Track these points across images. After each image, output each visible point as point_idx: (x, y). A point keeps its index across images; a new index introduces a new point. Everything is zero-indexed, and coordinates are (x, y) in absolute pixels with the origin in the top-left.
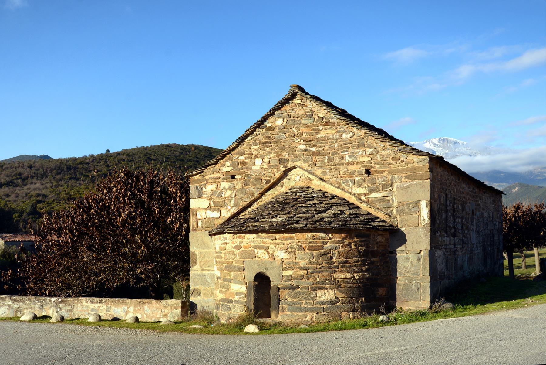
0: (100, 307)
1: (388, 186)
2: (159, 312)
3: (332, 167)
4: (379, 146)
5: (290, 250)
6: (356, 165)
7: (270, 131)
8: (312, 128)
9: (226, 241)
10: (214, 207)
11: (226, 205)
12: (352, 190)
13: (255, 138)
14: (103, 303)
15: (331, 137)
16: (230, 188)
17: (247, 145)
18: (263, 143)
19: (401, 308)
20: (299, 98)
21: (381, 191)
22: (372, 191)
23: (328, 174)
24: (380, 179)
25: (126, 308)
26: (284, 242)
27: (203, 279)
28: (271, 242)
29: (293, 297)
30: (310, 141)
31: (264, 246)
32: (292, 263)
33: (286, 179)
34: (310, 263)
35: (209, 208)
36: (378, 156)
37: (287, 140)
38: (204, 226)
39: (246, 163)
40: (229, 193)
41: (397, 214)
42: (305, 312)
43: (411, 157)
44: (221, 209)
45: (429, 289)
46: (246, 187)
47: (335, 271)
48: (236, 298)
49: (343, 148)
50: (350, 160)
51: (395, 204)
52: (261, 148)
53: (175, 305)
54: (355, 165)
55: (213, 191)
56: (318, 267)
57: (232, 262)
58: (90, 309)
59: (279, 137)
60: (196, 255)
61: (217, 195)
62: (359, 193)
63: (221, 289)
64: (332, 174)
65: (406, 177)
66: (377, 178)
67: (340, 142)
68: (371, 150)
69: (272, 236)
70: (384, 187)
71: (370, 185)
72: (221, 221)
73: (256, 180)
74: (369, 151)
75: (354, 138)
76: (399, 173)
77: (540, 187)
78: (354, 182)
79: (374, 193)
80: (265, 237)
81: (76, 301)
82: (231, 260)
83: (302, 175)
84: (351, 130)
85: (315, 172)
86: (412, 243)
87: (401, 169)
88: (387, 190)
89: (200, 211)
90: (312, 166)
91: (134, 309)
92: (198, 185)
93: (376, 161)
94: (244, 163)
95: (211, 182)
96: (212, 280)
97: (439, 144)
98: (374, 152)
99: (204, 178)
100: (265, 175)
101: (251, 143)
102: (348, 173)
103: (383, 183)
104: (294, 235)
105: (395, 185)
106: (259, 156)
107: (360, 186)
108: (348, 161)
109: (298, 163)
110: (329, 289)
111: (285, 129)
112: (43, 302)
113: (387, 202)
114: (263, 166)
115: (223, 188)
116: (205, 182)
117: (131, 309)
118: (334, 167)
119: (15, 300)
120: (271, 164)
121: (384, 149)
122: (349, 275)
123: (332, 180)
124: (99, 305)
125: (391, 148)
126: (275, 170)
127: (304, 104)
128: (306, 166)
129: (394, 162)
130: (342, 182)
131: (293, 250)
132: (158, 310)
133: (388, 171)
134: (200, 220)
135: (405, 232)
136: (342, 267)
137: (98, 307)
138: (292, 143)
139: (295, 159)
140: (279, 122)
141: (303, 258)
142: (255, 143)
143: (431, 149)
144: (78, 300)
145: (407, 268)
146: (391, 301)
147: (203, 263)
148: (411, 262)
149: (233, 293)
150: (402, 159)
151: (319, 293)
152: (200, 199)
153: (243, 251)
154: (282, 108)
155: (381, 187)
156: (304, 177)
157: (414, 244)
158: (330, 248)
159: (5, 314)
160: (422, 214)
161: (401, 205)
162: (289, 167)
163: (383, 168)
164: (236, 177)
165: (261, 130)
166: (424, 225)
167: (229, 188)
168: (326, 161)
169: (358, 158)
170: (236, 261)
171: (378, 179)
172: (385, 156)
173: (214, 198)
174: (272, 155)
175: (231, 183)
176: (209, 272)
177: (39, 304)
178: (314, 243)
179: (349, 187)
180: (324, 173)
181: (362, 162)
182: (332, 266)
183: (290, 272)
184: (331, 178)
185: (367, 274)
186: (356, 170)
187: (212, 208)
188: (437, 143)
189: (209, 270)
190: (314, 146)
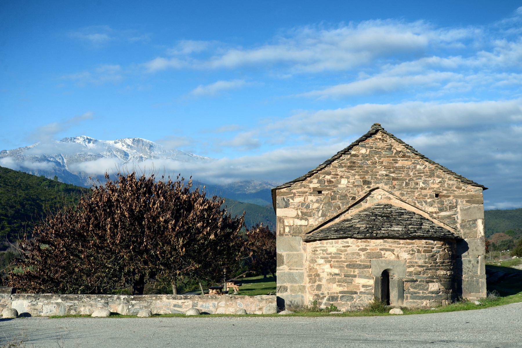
0: (184, 303)
1: (454, 208)
2: (254, 306)
3: (409, 190)
4: (445, 177)
5: (412, 253)
6: (429, 190)
7: (354, 158)
8: (391, 159)
9: (347, 245)
11: (314, 215)
13: (340, 162)
14: (189, 299)
15: (408, 167)
16: (317, 201)
17: (333, 167)
18: (349, 167)
19: (466, 298)
20: (380, 134)
21: (448, 211)
22: (441, 210)
23: (405, 195)
24: (447, 202)
25: (217, 303)
26: (407, 246)
28: (397, 246)
29: (415, 288)
30: (390, 168)
33: (370, 197)
34: (425, 263)
35: (297, 217)
37: (370, 166)
38: (292, 232)
39: (333, 182)
40: (316, 205)
41: (461, 229)
42: (422, 299)
43: (470, 187)
44: (309, 218)
45: (486, 284)
46: (333, 201)
47: (439, 269)
48: (363, 290)
49: (417, 176)
50: (424, 186)
51: (459, 221)
52: (346, 170)
53: (270, 300)
54: (427, 190)
55: (300, 203)
56: (429, 265)
57: (357, 261)
58: (173, 305)
59: (363, 163)
60: (283, 256)
61: (305, 206)
62: (431, 211)
64: (409, 195)
65: (467, 202)
66: (444, 200)
67: (415, 171)
68: (440, 179)
69: (398, 241)
70: (451, 208)
71: (439, 205)
74: (438, 180)
75: (426, 169)
77: (240, 203)
78: (426, 202)
79: (443, 211)
80: (391, 242)
81: (155, 298)
82: (354, 260)
83: (384, 195)
84: (424, 163)
85: (394, 193)
88: (453, 210)
90: (392, 188)
91: (226, 305)
92: (285, 197)
93: (444, 188)
94: (330, 182)
95: (299, 196)
96: (300, 278)
97: (132, 145)
98: (442, 181)
99: (291, 191)
100: (350, 193)
101: (337, 166)
102: (422, 195)
103: (450, 205)
104: (414, 241)
105: (459, 207)
106: (344, 177)
107: (432, 206)
109: (380, 185)
111: (368, 157)
112: (109, 299)
113: (453, 219)
114: (349, 186)
115: (311, 201)
116: (293, 195)
117: (223, 303)
118: (410, 190)
119: (67, 298)
120: (356, 184)
121: (450, 179)
122: (445, 272)
123: (409, 200)
124: (183, 301)
125: (455, 180)
126: (360, 189)
127: (384, 139)
128: (386, 187)
129: (458, 190)
131: (413, 252)
132: (252, 304)
133: (453, 196)
134: (287, 227)
135: (467, 242)
136: (442, 266)
137: (182, 303)
138: (374, 169)
139: (378, 181)
140: (363, 151)
141: (420, 259)
142: (341, 166)
143: (124, 151)
144: (156, 297)
145: (470, 268)
148: (472, 264)
149: (358, 286)
150: (463, 188)
151: (431, 285)
152: (286, 209)
153: (369, 252)
154: (366, 140)
155: (448, 208)
156: (385, 197)
157: (474, 251)
158: (436, 251)
159: (50, 313)
160: (479, 229)
161: (463, 221)
165: (346, 156)
166: (481, 237)
167: (316, 201)
168: (404, 185)
171: (446, 201)
173: (301, 209)
174: (357, 177)
175: (318, 197)
176: (297, 271)
177: (103, 301)
178: (427, 248)
180: (402, 194)
181: (433, 188)
182: (437, 265)
183: (412, 269)
184: (408, 199)
188: (130, 144)
189: (297, 270)
190: (394, 172)
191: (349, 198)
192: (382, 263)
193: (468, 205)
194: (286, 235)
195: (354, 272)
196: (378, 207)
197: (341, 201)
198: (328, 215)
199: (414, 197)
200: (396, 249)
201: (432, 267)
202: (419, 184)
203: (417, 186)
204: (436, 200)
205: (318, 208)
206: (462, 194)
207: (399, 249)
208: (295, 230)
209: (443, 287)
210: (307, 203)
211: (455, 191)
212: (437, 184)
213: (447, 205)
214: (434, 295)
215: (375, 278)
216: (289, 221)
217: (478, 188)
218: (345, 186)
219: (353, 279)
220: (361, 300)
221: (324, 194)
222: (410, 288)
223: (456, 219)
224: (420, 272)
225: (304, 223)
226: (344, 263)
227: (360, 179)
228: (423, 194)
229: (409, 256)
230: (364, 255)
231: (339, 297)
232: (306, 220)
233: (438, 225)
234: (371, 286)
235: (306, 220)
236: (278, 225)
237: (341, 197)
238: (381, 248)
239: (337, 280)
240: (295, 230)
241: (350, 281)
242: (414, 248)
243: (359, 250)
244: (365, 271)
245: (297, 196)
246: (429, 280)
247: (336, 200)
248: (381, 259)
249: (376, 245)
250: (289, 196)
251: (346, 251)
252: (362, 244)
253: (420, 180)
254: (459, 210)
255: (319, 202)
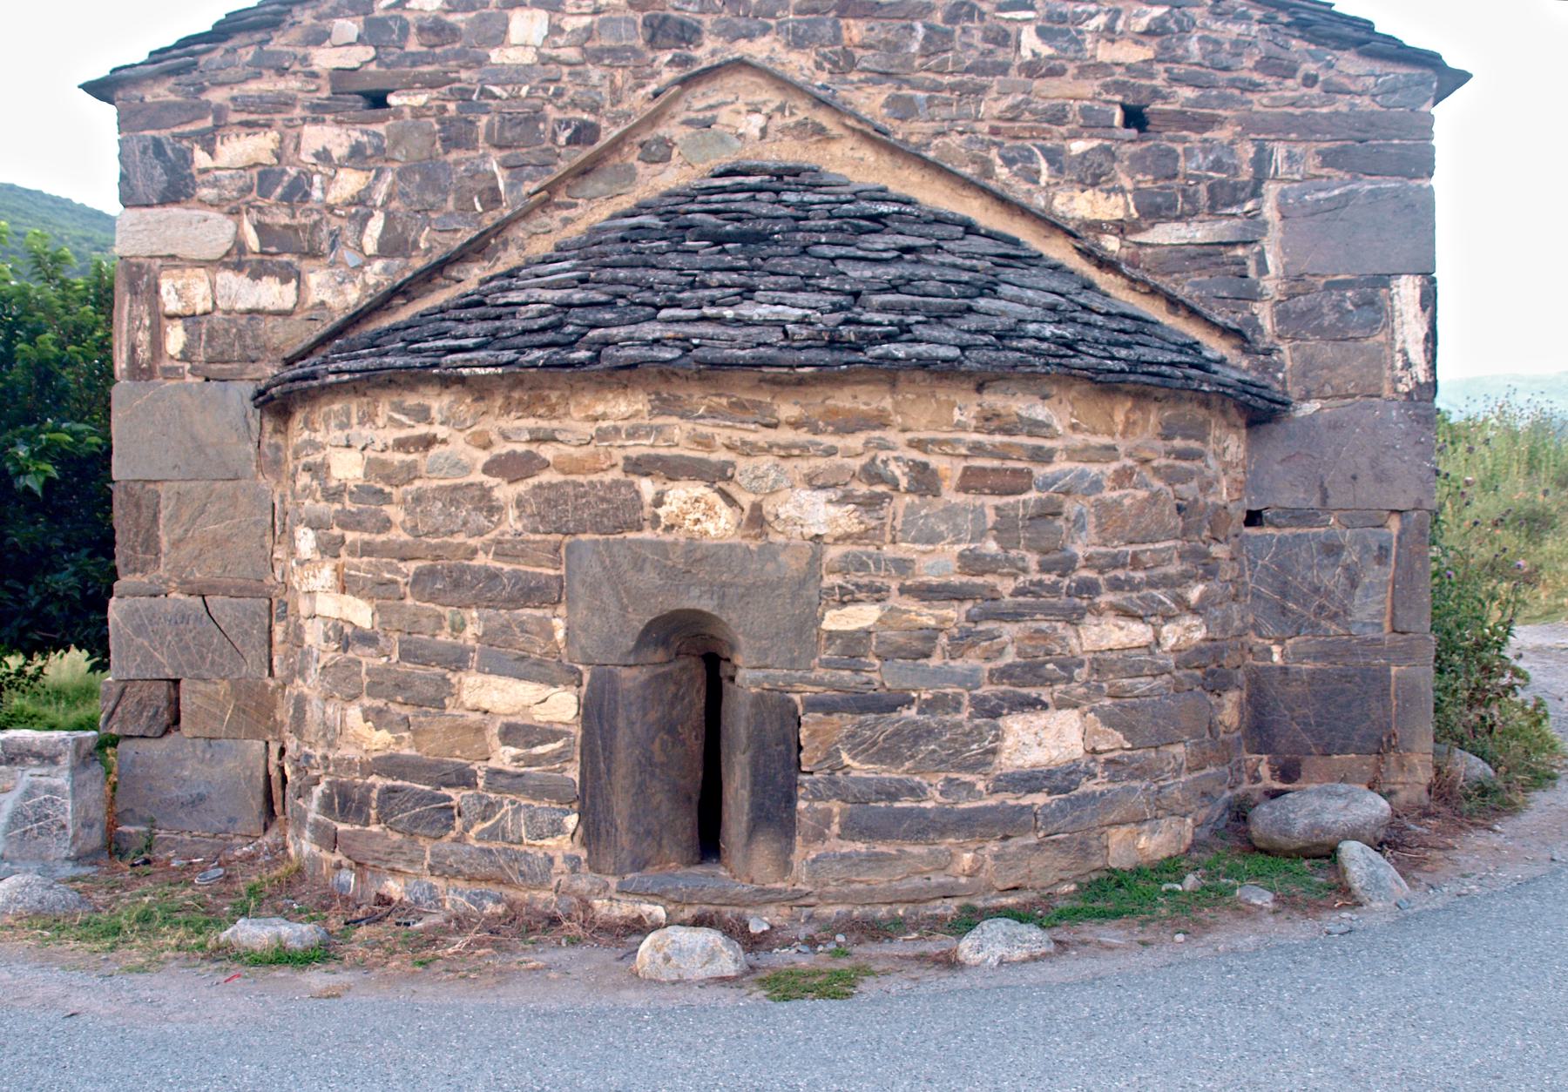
1: (1242, 196)
6: (1075, 78)
9: (422, 429)
10: (262, 253)
12: (1050, 201)
16: (357, 156)
22: (1154, 210)
26: (828, 440)
27: (189, 637)
29: (887, 753)
31: (701, 460)
32: (877, 563)
34: (971, 562)
35: (235, 259)
36: (1194, 45)
38: (201, 356)
39: (454, 32)
40: (350, 182)
43: (1350, 64)
44: (305, 265)
46: (454, 156)
48: (504, 756)
50: (1046, 51)
51: (1271, 285)
55: (255, 172)
57: (475, 552)
61: (279, 190)
63: (380, 703)
65: (1328, 159)
66: (1179, 148)
70: (1223, 197)
71: (1147, 181)
72: (304, 334)
73: (509, 121)
76: (1293, 136)
79: (1169, 219)
82: (460, 538)
86: (1354, 478)
87: (1304, 115)
88: (1234, 210)
89: (175, 272)
90: (835, 64)
93: (1180, 69)
100: (566, 99)
105: (1271, 190)
108: (1034, 54)
110: (1058, 708)
113: (1234, 268)
114: (554, 53)
115: (317, 155)
116: (209, 122)
129: (1270, 81)
130: (1002, 157)
131: (880, 489)
134: (179, 323)
139: (742, 23)
141: (932, 538)
145: (1328, 594)
146: (1247, 756)
147: (188, 549)
151: (1016, 726)
152: (174, 210)
153: (551, 486)
156: (791, 121)
160: (1399, 337)
162: (705, 65)
163: (1215, 103)
164: (393, 100)
166: (1409, 394)
169: (1089, 46)
170: (499, 542)
171: (1188, 154)
172: (1227, 46)
173: (260, 210)
175: (364, 132)
179: (1036, 182)
180: (903, 109)
183: (863, 616)
184: (938, 134)
185: (1198, 628)
186: (1077, 105)
187: (250, 257)
191: (555, 134)
192: (638, 564)
193: (1339, 184)
194: (170, 373)
195: (458, 628)
196: (727, 182)
197: (506, 153)
198: (423, 245)
199: (979, 126)
200: (743, 463)
201: (1030, 599)
202: (1012, 42)
203: (1001, 55)
204: (1129, 144)
205: (361, 200)
206: (1298, 112)
207: (765, 462)
208: (219, 343)
209: (1119, 735)
210: (293, 172)
211: (1254, 87)
212: (1136, 42)
213: (1199, 179)
214: (1040, 799)
215: (586, 678)
216: (186, 287)
217: (1403, 71)
218: (528, 57)
219: (449, 675)
220: (492, 834)
221: (398, 111)
222: (846, 758)
223: (1252, 273)
224: (930, 635)
225: (272, 293)
226: (401, 565)
227: (631, 13)
228: (1041, 105)
229: (846, 519)
230: (520, 503)
231: (374, 794)
232: (287, 274)
233: (1183, 335)
234: (553, 735)
235: (285, 281)
236: (121, 308)
237: (502, 127)
238: (633, 452)
239: (366, 680)
240: (219, 343)
241: (430, 691)
242: (883, 455)
243: (487, 470)
244: (521, 624)
245: (236, 129)
246: (1003, 698)
247: (475, 148)
248: (631, 535)
249: (602, 435)
250: (188, 128)
251: (411, 472)
252: (510, 422)
253: (1021, 15)
254: (1270, 212)
255: (371, 162)
